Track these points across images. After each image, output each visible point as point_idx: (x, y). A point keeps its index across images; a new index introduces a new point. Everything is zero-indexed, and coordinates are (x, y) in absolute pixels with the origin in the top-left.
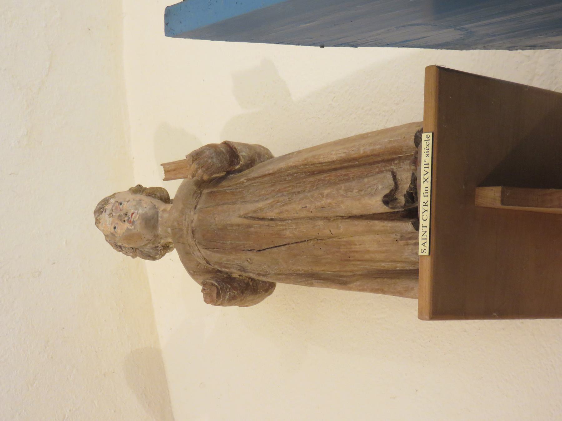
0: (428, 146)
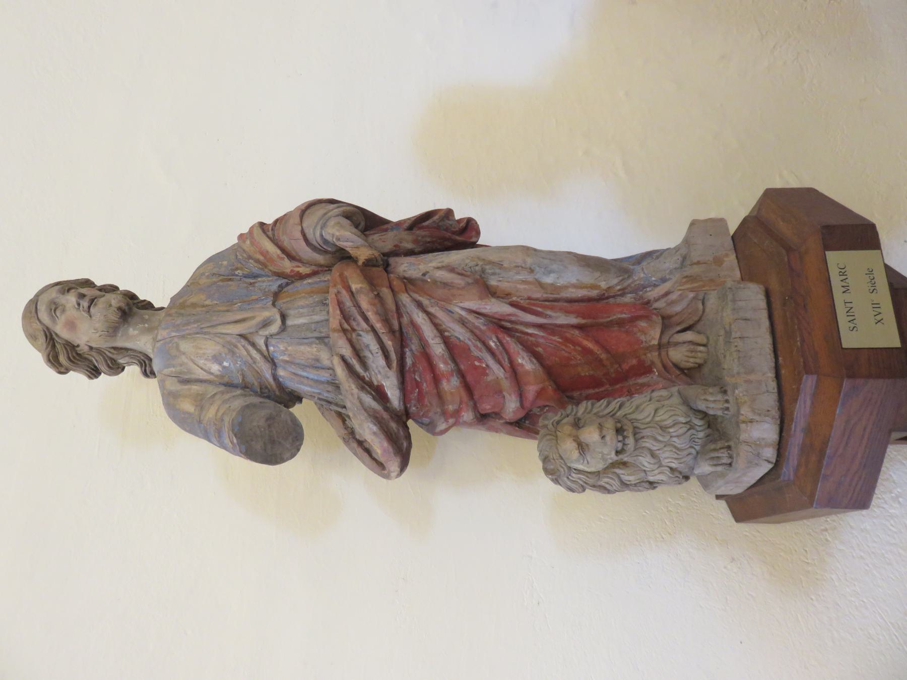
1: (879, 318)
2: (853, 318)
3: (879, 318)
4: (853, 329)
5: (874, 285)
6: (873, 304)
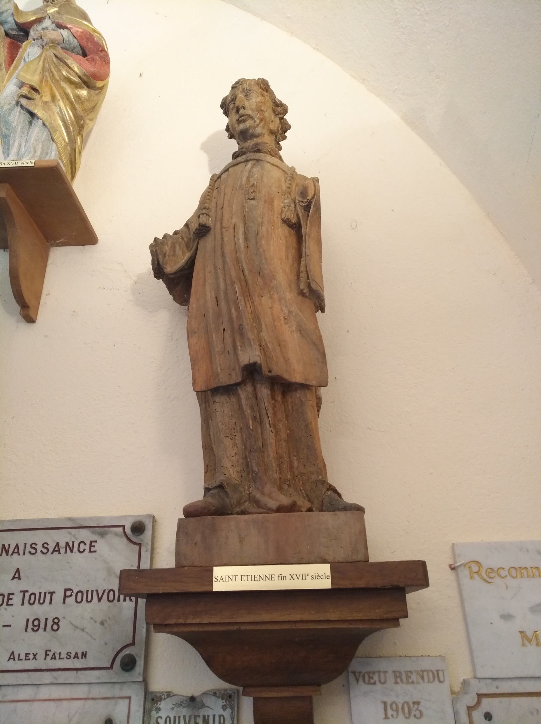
0: (320, 577)
1: (295, 577)
2: (224, 580)
3: (295, 577)
4: (216, 578)
5: (316, 578)
6: (305, 574)
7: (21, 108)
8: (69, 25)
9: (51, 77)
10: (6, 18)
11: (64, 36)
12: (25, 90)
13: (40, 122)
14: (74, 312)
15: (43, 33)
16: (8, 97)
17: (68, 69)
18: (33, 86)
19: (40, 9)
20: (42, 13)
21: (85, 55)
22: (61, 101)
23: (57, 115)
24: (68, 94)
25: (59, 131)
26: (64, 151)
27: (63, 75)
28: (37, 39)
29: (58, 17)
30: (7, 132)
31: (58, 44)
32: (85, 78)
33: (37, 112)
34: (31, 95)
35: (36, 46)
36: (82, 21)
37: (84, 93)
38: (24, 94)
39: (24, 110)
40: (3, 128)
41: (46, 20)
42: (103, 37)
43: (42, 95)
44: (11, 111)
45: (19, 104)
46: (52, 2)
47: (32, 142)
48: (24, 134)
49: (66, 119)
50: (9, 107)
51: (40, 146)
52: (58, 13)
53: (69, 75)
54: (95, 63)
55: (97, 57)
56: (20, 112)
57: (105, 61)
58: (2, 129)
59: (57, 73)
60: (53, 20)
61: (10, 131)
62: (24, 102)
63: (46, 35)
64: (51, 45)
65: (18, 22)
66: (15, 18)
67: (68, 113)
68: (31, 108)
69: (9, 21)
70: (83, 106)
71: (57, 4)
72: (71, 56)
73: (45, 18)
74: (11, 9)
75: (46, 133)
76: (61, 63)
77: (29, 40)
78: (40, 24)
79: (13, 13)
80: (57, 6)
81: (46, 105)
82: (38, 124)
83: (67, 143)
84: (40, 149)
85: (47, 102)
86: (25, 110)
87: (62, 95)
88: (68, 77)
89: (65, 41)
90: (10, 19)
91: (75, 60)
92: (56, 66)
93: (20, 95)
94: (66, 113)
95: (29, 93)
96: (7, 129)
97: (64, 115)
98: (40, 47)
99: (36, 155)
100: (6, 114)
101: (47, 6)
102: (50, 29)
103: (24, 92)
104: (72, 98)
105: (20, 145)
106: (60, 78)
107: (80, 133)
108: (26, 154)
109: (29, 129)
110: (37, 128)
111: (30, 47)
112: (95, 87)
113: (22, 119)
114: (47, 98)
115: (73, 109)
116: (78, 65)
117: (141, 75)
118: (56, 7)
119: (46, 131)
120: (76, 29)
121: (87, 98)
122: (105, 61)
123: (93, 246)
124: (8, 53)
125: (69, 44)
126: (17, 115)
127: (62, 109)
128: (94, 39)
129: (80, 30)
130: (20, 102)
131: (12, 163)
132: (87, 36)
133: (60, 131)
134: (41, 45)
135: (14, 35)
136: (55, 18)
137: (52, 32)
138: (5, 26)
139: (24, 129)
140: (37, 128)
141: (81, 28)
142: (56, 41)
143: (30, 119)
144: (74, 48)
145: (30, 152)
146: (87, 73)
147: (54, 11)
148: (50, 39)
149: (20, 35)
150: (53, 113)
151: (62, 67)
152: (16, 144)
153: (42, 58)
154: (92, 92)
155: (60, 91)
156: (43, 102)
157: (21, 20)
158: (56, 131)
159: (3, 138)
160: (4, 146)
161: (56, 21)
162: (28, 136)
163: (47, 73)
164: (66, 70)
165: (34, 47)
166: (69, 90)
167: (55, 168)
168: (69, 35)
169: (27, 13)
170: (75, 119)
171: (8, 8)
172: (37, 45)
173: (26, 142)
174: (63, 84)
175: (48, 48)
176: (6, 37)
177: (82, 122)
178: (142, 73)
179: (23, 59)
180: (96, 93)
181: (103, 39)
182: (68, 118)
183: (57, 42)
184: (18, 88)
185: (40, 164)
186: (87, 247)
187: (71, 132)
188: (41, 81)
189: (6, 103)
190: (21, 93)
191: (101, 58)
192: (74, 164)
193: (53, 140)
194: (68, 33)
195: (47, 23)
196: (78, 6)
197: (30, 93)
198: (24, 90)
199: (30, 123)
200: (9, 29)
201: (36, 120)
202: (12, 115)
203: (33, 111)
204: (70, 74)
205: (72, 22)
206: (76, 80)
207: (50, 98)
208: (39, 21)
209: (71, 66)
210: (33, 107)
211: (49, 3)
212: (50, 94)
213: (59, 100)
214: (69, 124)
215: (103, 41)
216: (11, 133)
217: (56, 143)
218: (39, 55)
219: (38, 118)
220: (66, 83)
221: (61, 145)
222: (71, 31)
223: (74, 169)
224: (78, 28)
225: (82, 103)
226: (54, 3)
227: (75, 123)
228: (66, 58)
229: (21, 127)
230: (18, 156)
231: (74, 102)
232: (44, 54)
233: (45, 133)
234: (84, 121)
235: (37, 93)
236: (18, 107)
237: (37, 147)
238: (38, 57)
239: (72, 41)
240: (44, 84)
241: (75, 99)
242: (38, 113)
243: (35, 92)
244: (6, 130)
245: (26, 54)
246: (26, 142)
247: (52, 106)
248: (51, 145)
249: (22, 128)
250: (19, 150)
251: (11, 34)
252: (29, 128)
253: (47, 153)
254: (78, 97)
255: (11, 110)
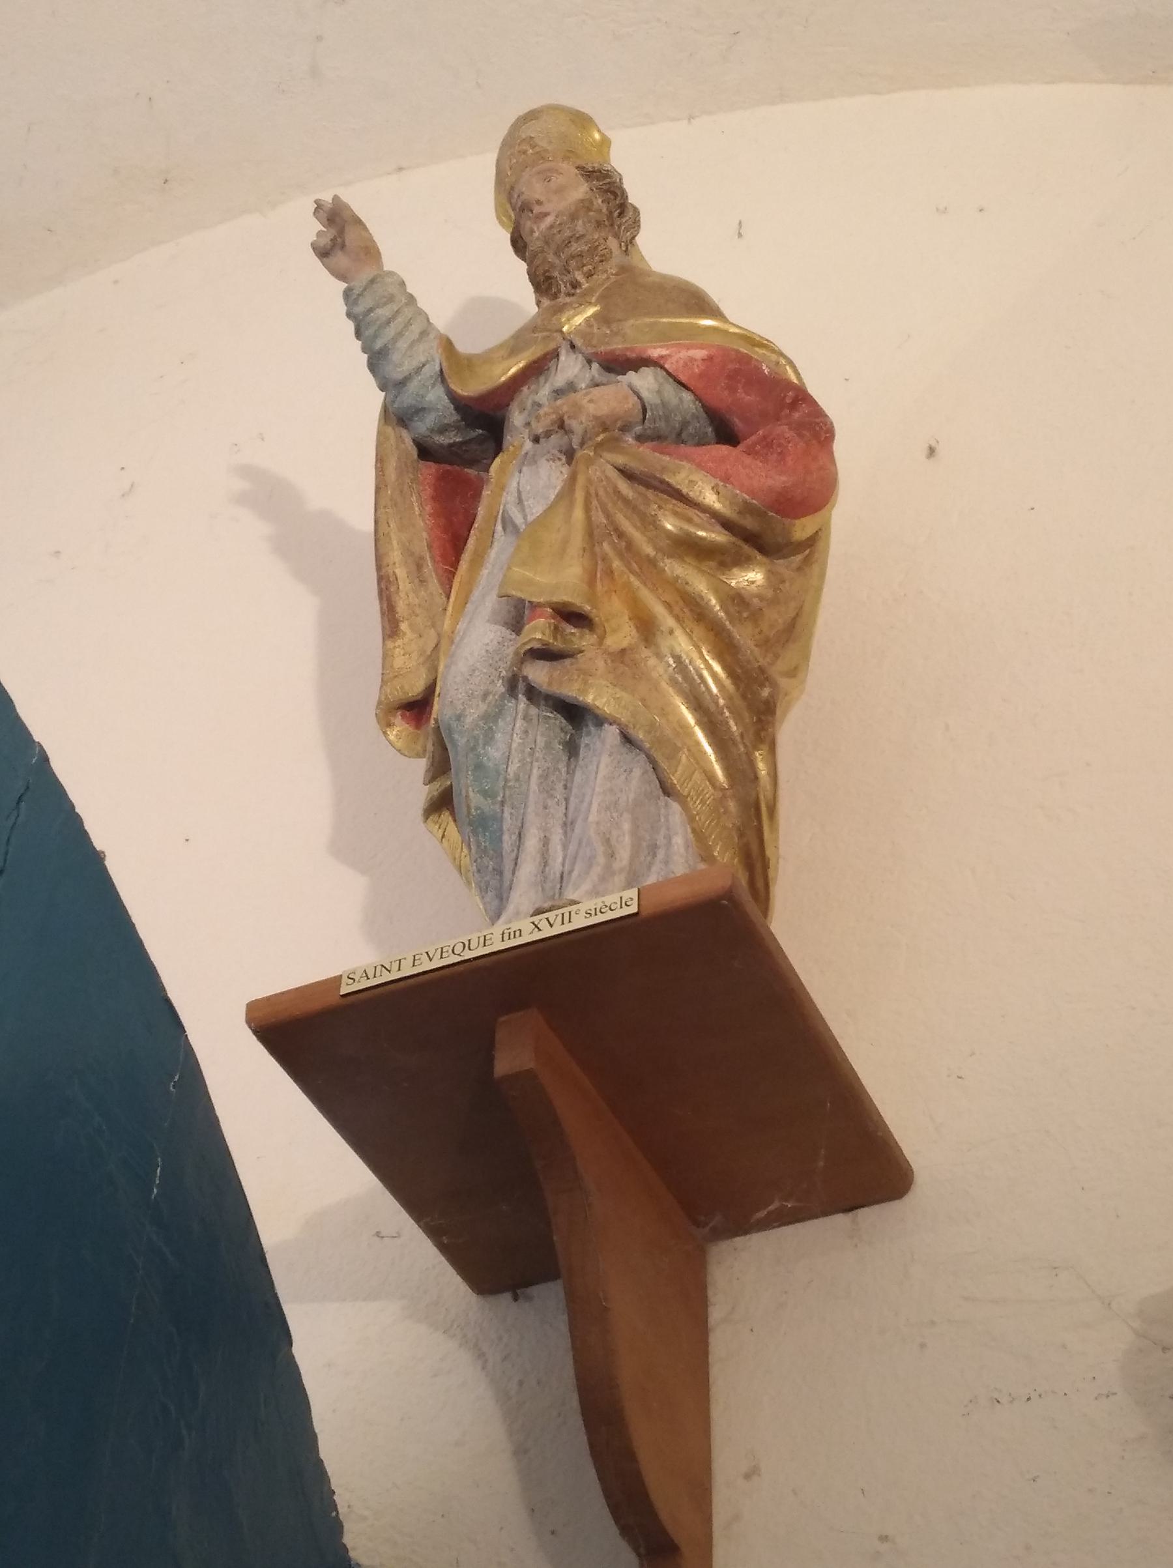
7: (529, 699)
8: (655, 348)
9: (621, 556)
10: (417, 395)
11: (645, 394)
12: (538, 631)
13: (611, 733)
14: (884, 1538)
15: (565, 408)
16: (477, 673)
17: (681, 507)
18: (565, 604)
19: (534, 326)
20: (544, 338)
21: (726, 435)
22: (678, 632)
23: (671, 690)
24: (698, 600)
25: (685, 750)
26: (717, 824)
27: (668, 534)
28: (548, 434)
29: (606, 335)
30: (487, 805)
31: (625, 429)
32: (749, 523)
33: (594, 700)
34: (565, 641)
35: (543, 462)
36: (692, 321)
37: (751, 578)
38: (537, 645)
39: (543, 702)
40: (471, 794)
41: (562, 358)
42: (781, 354)
43: (605, 631)
44: (496, 722)
45: (521, 686)
46: (573, 291)
47: (593, 817)
48: (552, 796)
49: (708, 697)
50: (483, 707)
51: (626, 826)
52: (602, 319)
53: (692, 529)
54: (780, 454)
55: (783, 430)
56: (526, 717)
57: (816, 436)
58: (467, 796)
59: (643, 533)
60: (590, 350)
61: (499, 799)
62: (538, 673)
63: (577, 408)
64: (599, 439)
65: (464, 398)
66: (453, 386)
67: (709, 668)
68: (570, 691)
69: (430, 402)
70: (757, 630)
71: (590, 292)
72: (687, 458)
73: (555, 354)
74: (434, 361)
75: (639, 769)
76: (650, 494)
77: (511, 448)
78: (542, 379)
79: (441, 371)
80: (594, 300)
81: (622, 662)
82: (603, 742)
83: (723, 789)
84: (627, 839)
85: (623, 651)
86: (546, 705)
87: (677, 610)
88: (689, 535)
89: (651, 410)
90: (436, 396)
91: (700, 466)
92: (635, 509)
93: (525, 654)
94: (706, 674)
95: (555, 638)
96: (485, 794)
97: (699, 681)
98: (560, 459)
99: (617, 865)
100: (476, 739)
101: (560, 309)
102: (583, 386)
103: (539, 636)
104: (718, 608)
105: (546, 842)
106: (657, 549)
107: (763, 734)
108: (575, 873)
109: (568, 773)
110: (605, 760)
111: (520, 472)
112: (789, 543)
113: (541, 741)
114: (623, 635)
115: (726, 649)
116: (714, 481)
117: (932, 451)
118: (590, 303)
119: (638, 762)
120: (684, 354)
121: (770, 594)
122: (816, 436)
123: (897, 1202)
124: (435, 515)
125: (667, 418)
126: (517, 730)
127: (687, 661)
128: (759, 370)
129: (699, 354)
130: (525, 678)
131: (547, 919)
132: (731, 366)
133: (689, 750)
134: (561, 451)
135: (451, 445)
136: (594, 342)
137: (596, 391)
138: (419, 423)
139: (553, 778)
140: (605, 760)
141: (701, 347)
142: (616, 421)
143: (566, 733)
144: (685, 424)
145: (590, 862)
146: (754, 501)
147: (587, 320)
148: (596, 418)
149: (470, 441)
150: (656, 687)
151: (660, 507)
152: (532, 843)
153: (579, 495)
154: (781, 564)
155: (668, 597)
156: (610, 654)
157: (471, 388)
158: (673, 756)
159: (475, 832)
160: (479, 860)
161: (602, 349)
162: (572, 799)
163: (605, 545)
164: (676, 514)
165: (534, 467)
166: (701, 586)
167: (725, 902)
168: (661, 385)
169: (487, 358)
170: (737, 687)
171: (423, 359)
172: (549, 456)
173: (568, 826)
174: (675, 568)
175: (592, 454)
176: (421, 462)
177: (765, 693)
178: (938, 442)
179: (499, 520)
180: (794, 566)
181: (783, 361)
182: (715, 690)
183: (619, 424)
184: (507, 633)
185: (654, 905)
186: (868, 1215)
187: (735, 743)
188: (591, 581)
189: (471, 696)
190: (525, 644)
191: (799, 428)
192: (758, 866)
193: (667, 790)
194: (656, 379)
195: (569, 368)
196: (664, 276)
197: (559, 637)
198: (535, 629)
199: (572, 749)
200: (432, 431)
201: (592, 729)
202: (498, 736)
203: (581, 699)
204: (689, 520)
205: (664, 336)
206: (717, 536)
207: (634, 632)
208: (537, 369)
209: (691, 493)
210: (576, 686)
211: (562, 299)
212: (630, 619)
213: (671, 632)
214: (722, 713)
215: (788, 368)
216: (503, 803)
217: (682, 800)
218: (563, 488)
219: (600, 721)
220: (681, 558)
221: (703, 802)
222: (667, 366)
223: (760, 884)
224: (688, 348)
225: (755, 616)
226: (578, 291)
227: (739, 702)
228: (664, 469)
229: (540, 771)
230: (543, 889)
231: (727, 623)
232: (581, 481)
233: (637, 772)
234: (774, 685)
235: (583, 628)
236: (516, 699)
237: (615, 833)
238: (560, 497)
239: (674, 401)
240: (599, 587)
241: (726, 613)
242: (597, 703)
243: (575, 627)
244: (482, 799)
245: (509, 499)
246: (565, 824)
247: (646, 659)
248: (663, 811)
249: (544, 777)
250: (546, 864)
251: (441, 446)
252: (568, 765)
253: (653, 849)
254: (737, 600)
255: (491, 718)
